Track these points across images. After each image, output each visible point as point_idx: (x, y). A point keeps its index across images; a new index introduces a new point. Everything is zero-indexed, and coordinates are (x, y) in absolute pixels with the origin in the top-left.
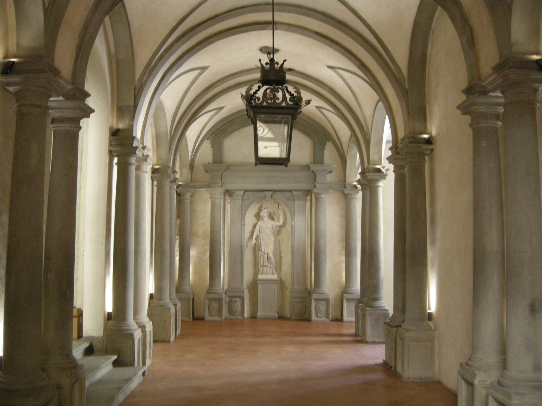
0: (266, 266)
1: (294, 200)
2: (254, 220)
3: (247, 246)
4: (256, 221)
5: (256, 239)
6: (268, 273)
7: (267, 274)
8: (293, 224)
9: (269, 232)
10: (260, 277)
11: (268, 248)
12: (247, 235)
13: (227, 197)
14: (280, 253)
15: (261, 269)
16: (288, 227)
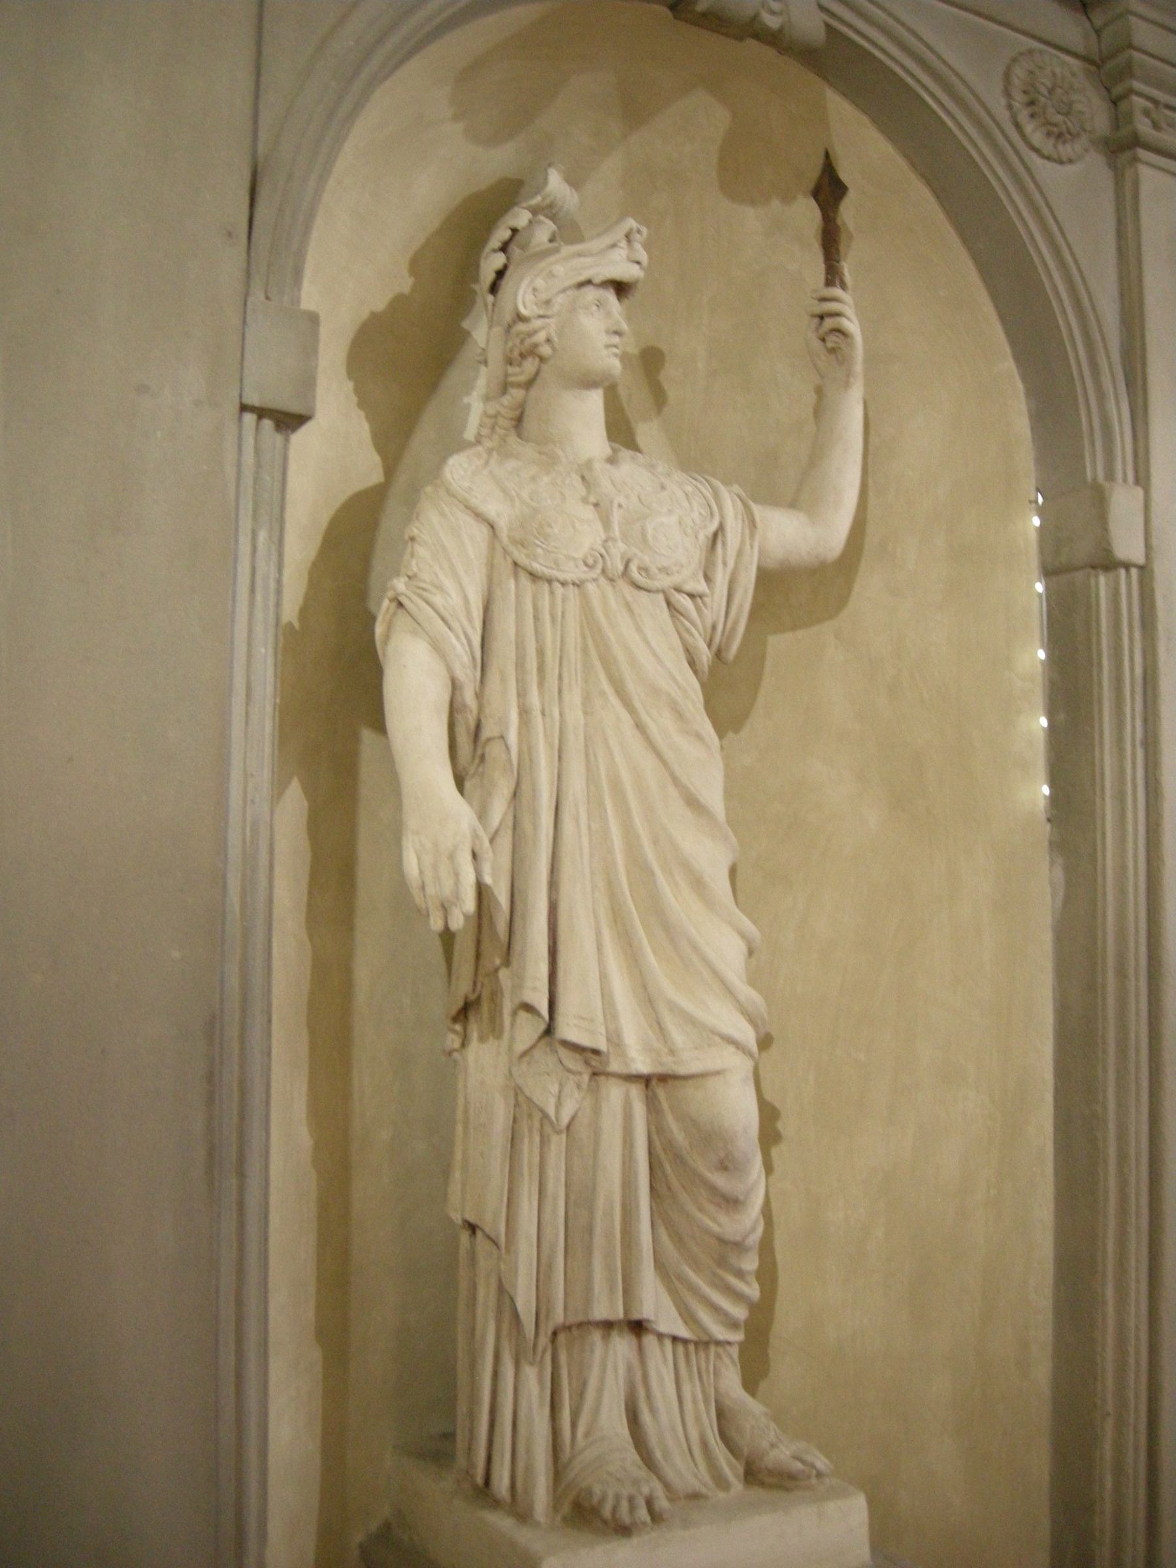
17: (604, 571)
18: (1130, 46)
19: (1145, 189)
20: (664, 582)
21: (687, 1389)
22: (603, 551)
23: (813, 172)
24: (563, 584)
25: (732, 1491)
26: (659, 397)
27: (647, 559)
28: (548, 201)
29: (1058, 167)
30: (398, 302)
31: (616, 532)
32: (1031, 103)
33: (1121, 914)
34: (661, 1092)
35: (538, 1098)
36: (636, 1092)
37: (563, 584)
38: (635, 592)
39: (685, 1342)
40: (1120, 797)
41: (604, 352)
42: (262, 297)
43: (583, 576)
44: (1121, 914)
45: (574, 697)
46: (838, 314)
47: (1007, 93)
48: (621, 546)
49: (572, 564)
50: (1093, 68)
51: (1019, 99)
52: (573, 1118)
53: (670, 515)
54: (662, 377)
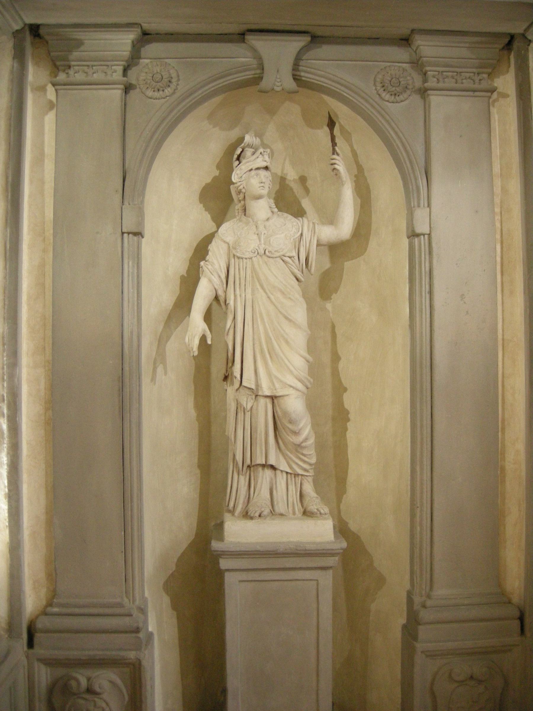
0: (273, 467)
1: (423, 92)
2: (199, 219)
3: (160, 357)
4: (210, 226)
5: (208, 317)
6: (280, 507)
7: (273, 513)
8: (422, 227)
9: (278, 275)
10: (238, 532)
11: (278, 365)
12: (157, 294)
13: (34, 74)
14: (339, 389)
15: (239, 483)
16: (388, 252)
17: (258, 253)
18: (421, 57)
19: (433, 104)
20: (277, 254)
21: (290, 487)
22: (257, 248)
23: (326, 120)
24: (246, 259)
25: (296, 516)
26: (307, 190)
27: (270, 249)
28: (246, 144)
29: (397, 104)
30: (215, 179)
31: (263, 242)
32: (383, 86)
33: (421, 349)
34: (275, 401)
35: (242, 403)
36: (269, 401)
37: (246, 259)
38: (269, 259)
39: (291, 474)
40: (421, 311)
41: (259, 189)
42: (128, 204)
43: (251, 256)
44: (421, 349)
45: (249, 291)
46: (335, 164)
47: (375, 85)
48: (263, 246)
49: (248, 253)
50: (415, 65)
51: (379, 86)
52: (252, 407)
53: (283, 232)
54: (307, 184)
